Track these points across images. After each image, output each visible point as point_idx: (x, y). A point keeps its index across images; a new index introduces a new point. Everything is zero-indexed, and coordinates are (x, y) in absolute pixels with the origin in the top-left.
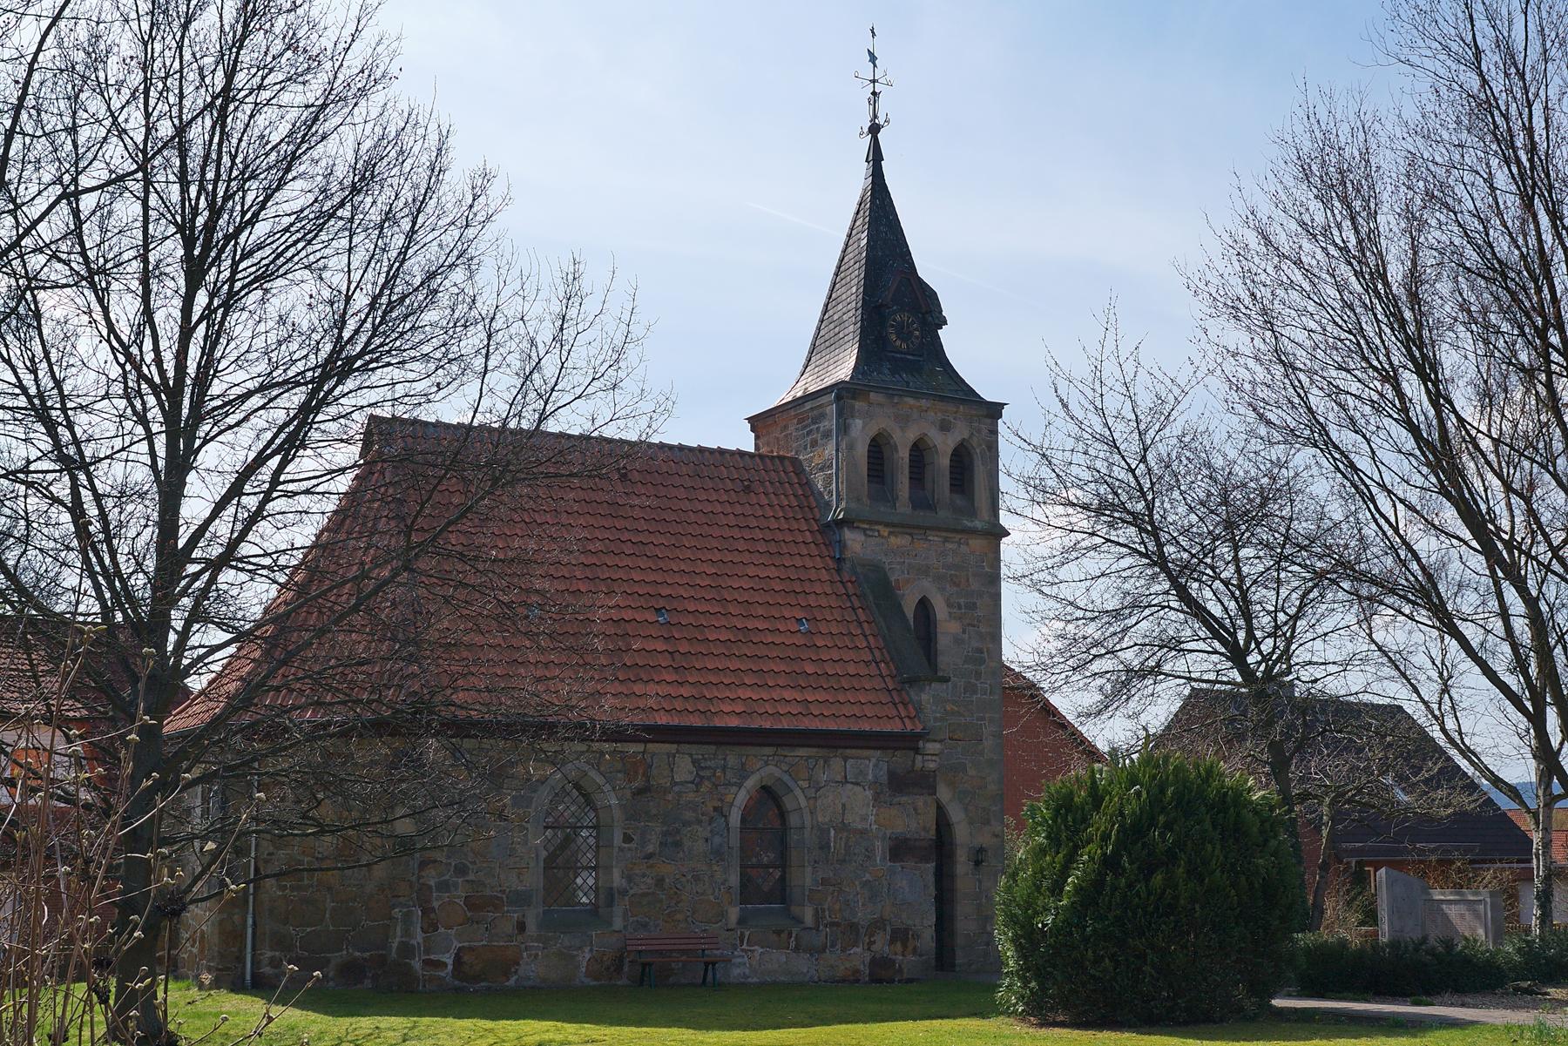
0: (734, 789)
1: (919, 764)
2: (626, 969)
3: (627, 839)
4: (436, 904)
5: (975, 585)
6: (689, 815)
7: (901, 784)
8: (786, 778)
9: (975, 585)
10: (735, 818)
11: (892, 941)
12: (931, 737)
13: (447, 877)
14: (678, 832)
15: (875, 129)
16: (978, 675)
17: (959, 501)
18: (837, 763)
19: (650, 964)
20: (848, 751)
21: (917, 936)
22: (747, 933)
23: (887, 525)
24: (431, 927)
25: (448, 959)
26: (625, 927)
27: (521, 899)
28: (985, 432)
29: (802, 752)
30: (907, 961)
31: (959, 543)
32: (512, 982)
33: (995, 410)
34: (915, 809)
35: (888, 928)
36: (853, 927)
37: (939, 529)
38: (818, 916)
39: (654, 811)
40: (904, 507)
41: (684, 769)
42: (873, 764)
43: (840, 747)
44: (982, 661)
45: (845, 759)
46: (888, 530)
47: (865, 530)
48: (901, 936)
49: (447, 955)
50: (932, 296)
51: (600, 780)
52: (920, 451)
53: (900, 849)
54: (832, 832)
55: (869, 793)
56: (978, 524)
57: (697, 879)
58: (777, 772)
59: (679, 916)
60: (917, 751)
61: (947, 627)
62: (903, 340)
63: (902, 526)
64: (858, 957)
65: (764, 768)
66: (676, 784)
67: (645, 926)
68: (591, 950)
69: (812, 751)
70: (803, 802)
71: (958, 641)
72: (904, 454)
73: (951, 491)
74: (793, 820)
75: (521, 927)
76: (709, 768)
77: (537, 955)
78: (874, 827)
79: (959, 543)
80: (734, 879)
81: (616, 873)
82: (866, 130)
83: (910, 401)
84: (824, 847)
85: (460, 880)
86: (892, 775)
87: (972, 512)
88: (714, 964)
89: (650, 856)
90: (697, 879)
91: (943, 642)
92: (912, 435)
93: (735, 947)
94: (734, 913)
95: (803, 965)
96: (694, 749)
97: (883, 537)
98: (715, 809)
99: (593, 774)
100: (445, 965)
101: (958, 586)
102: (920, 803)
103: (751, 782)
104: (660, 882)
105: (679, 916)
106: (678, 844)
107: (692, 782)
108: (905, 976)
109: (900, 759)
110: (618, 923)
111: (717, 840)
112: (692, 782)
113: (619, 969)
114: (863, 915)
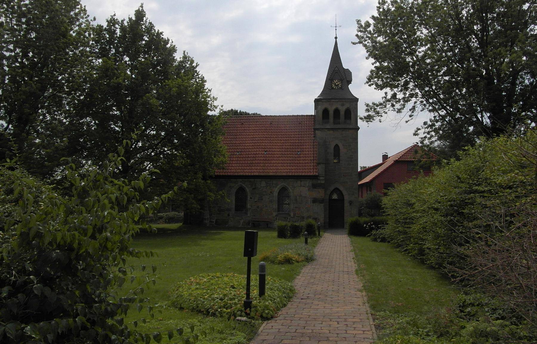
3: (251, 198)
7: (315, 186)
8: (287, 186)
18: (299, 182)
25: (214, 221)
29: (290, 180)
38: (294, 215)
41: (263, 184)
42: (308, 183)
45: (301, 181)
50: (351, 73)
52: (337, 111)
53: (315, 201)
55: (307, 189)
56: (351, 127)
61: (343, 150)
65: (281, 184)
75: (229, 215)
81: (248, 205)
84: (296, 200)
89: (256, 202)
91: (341, 154)
92: (334, 107)
93: (275, 221)
98: (271, 192)
104: (258, 207)
106: (262, 199)
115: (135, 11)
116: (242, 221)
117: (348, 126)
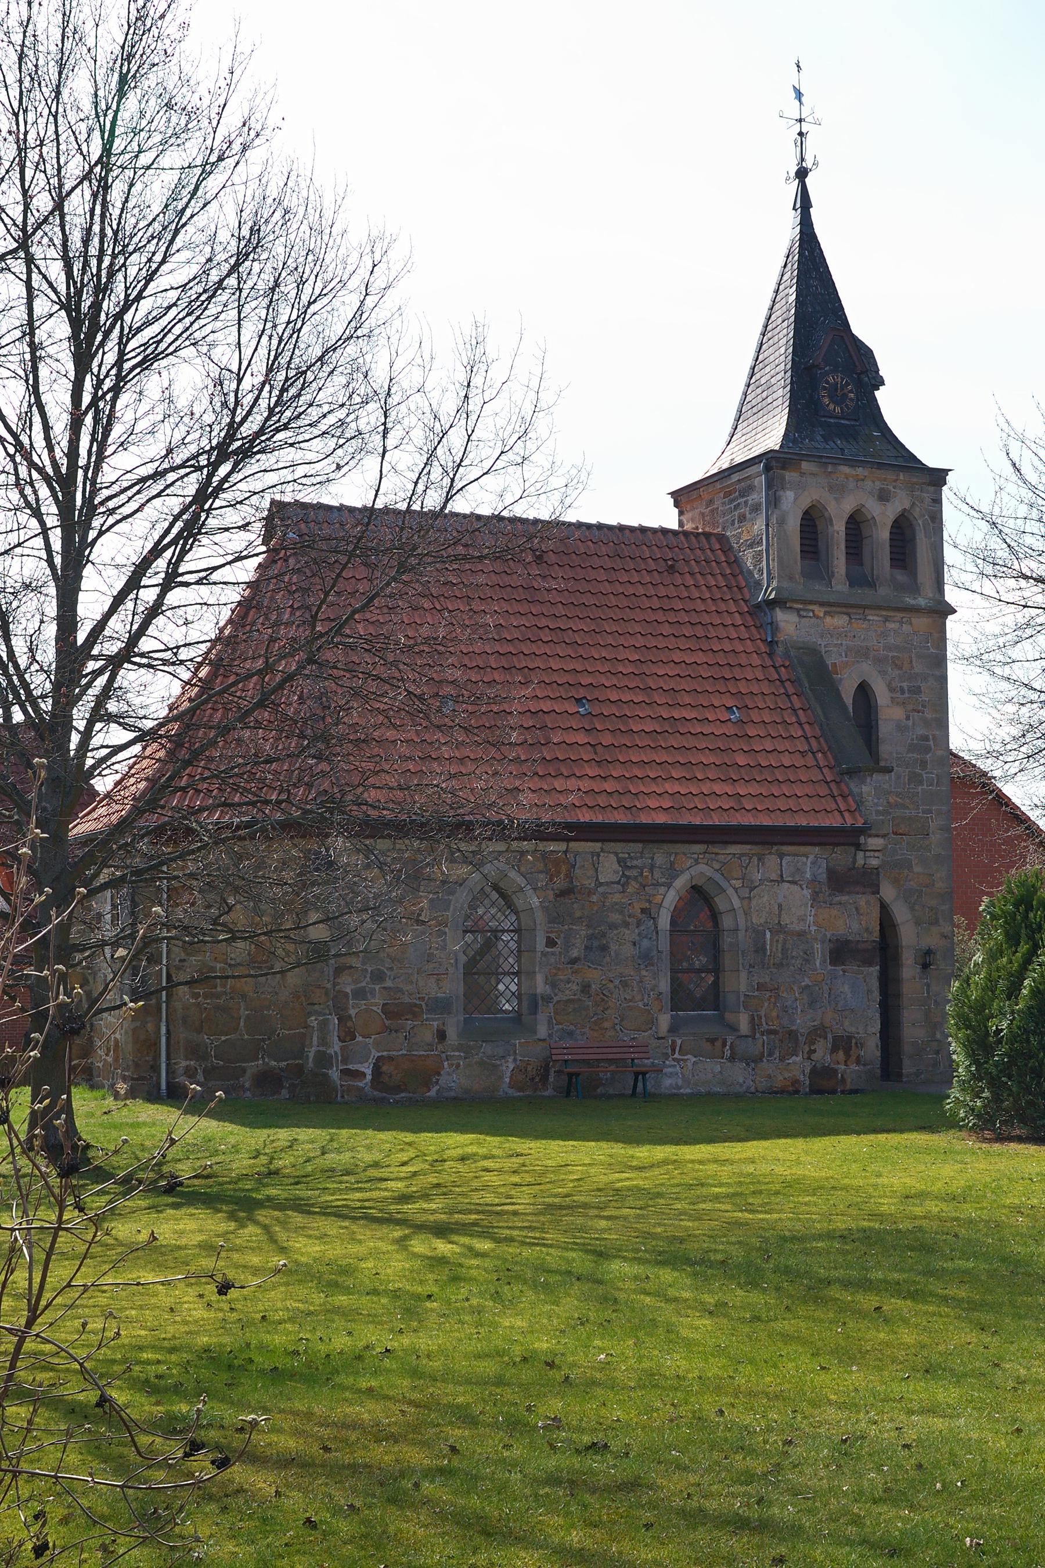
0: (662, 890)
1: (860, 862)
2: (551, 1079)
3: (551, 943)
4: (353, 1012)
5: (918, 668)
6: (616, 917)
8: (718, 877)
9: (918, 668)
10: (664, 921)
11: (834, 1049)
12: (873, 832)
13: (364, 984)
14: (604, 935)
15: (802, 174)
16: (924, 764)
17: (901, 577)
18: (772, 861)
19: (577, 1075)
20: (786, 849)
21: (860, 1045)
22: (679, 1042)
23: (822, 604)
24: (348, 1035)
25: (367, 1069)
26: (550, 1035)
27: (441, 1006)
28: (928, 501)
30: (850, 1071)
31: (901, 623)
32: (432, 1093)
33: (938, 477)
34: (857, 909)
35: (830, 1036)
36: (792, 1035)
37: (880, 608)
39: (578, 914)
40: (840, 585)
41: (609, 868)
43: (776, 844)
44: (927, 750)
45: (781, 856)
46: (823, 610)
47: (798, 610)
48: (844, 1044)
49: (366, 1065)
51: (521, 881)
52: (856, 524)
54: (768, 935)
55: (807, 893)
56: (922, 602)
57: (625, 984)
58: (709, 872)
59: (606, 1025)
60: (858, 847)
62: (837, 403)
63: (839, 605)
64: (798, 1067)
66: (601, 884)
67: (571, 1034)
68: (515, 1060)
69: (746, 848)
70: (736, 903)
71: (901, 728)
72: (839, 528)
73: (891, 566)
74: (727, 922)
75: (442, 1035)
76: (636, 867)
77: (458, 1066)
78: (813, 928)
79: (901, 623)
80: (664, 985)
81: (540, 978)
82: (792, 174)
83: (846, 470)
84: (760, 949)
85: (377, 987)
86: (831, 873)
87: (914, 589)
88: (644, 1074)
89: (574, 961)
90: (625, 984)
91: (885, 729)
92: (848, 506)
93: (666, 1056)
94: (664, 1021)
95: (739, 1075)
96: (618, 847)
97: (818, 617)
98: (643, 911)
99: (512, 874)
100: (364, 1075)
101: (901, 668)
102: (862, 903)
103: (681, 882)
104: (586, 988)
105: (606, 1025)
106: (604, 948)
107: (618, 883)
108: (848, 1087)
109: (841, 857)
110: (542, 1031)
111: (646, 943)
112: (618, 883)
113: (544, 1079)
114: (802, 1022)
115: (938, 477)
116: (509, 1065)
117: (910, 601)
